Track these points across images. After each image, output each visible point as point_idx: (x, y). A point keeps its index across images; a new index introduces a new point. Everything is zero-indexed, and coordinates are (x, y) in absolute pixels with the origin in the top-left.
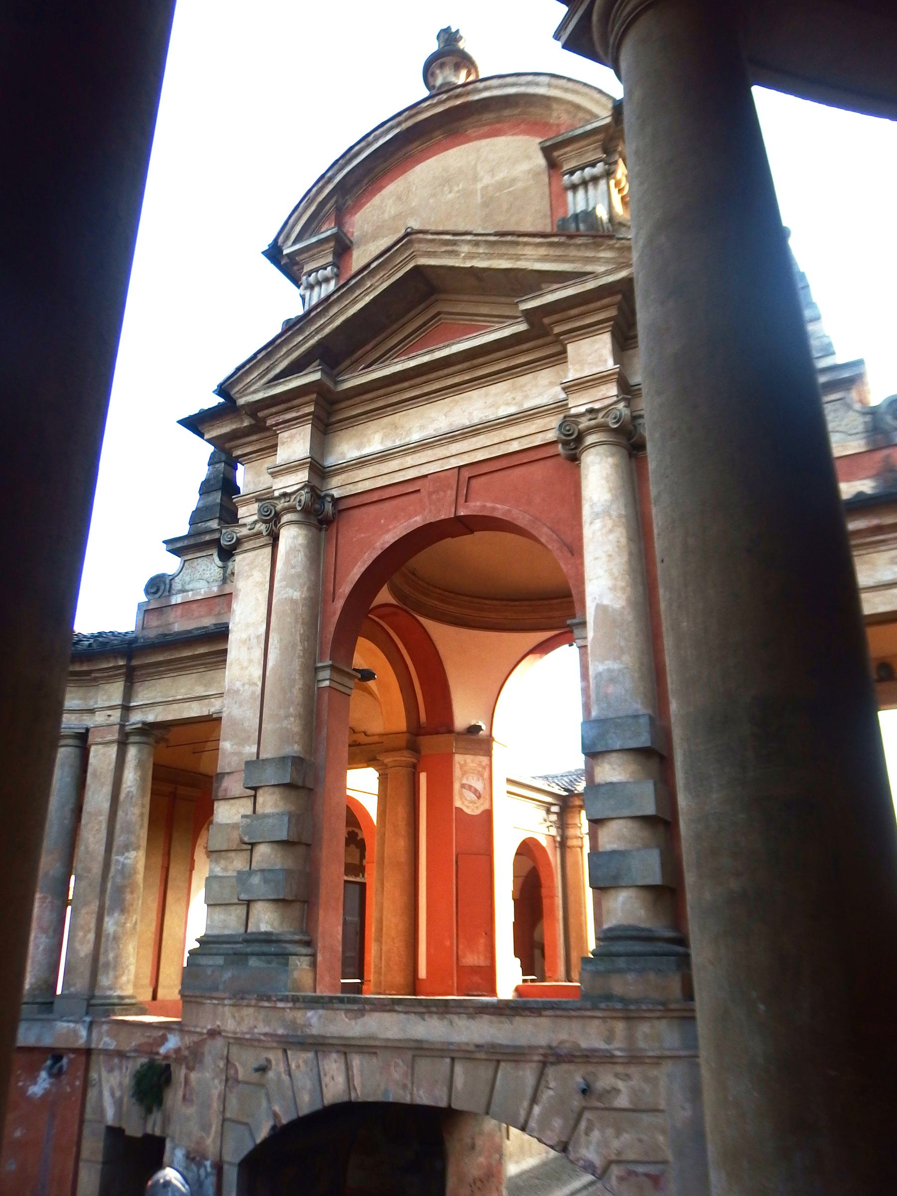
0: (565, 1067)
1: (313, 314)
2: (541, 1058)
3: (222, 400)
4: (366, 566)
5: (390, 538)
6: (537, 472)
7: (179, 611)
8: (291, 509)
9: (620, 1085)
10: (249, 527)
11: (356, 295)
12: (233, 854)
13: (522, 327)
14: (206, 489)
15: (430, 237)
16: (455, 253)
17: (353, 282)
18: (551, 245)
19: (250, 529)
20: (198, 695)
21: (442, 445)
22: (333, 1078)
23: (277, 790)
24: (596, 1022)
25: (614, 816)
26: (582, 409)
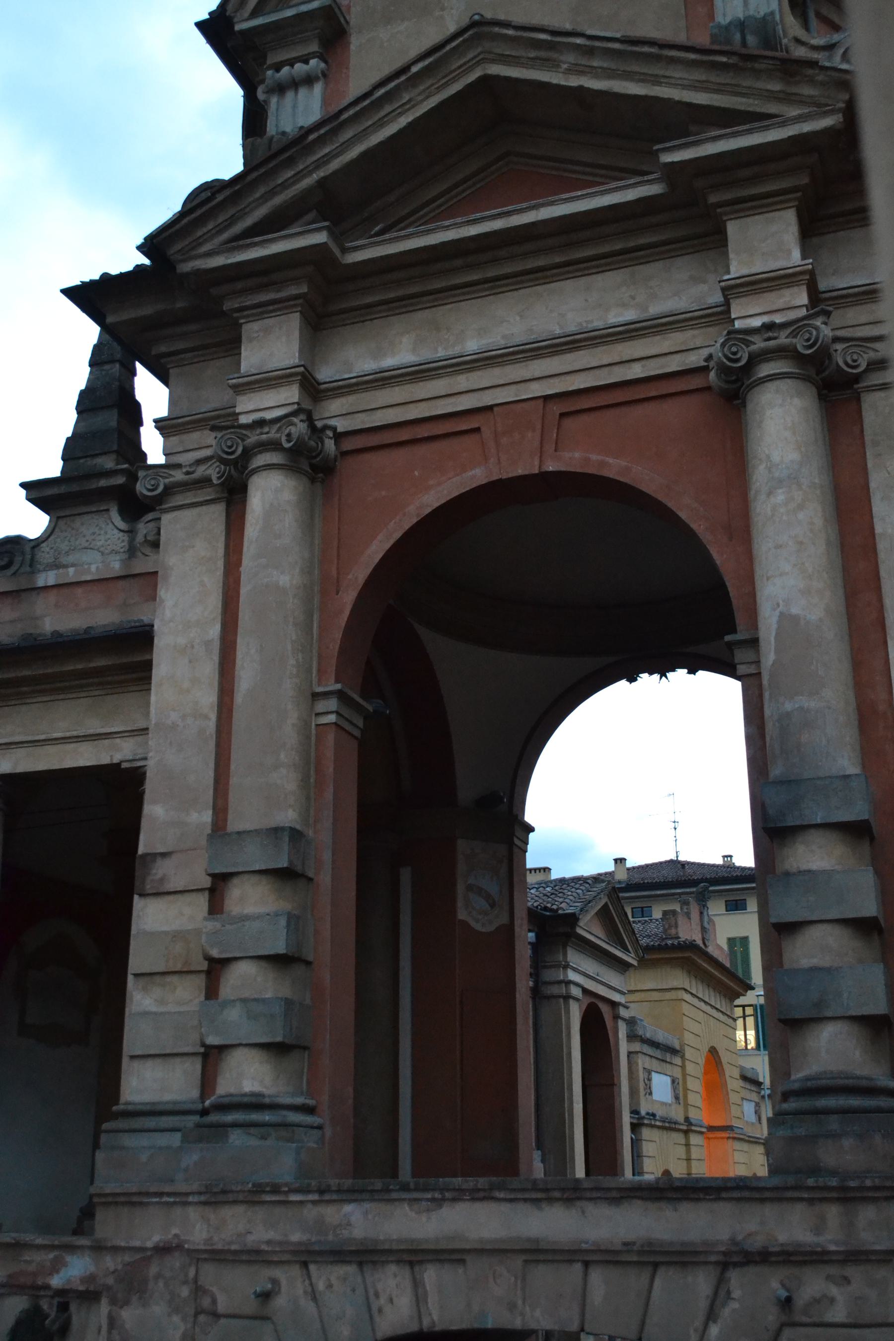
0: (752, 1270)
1: (312, 137)
2: (721, 1258)
3: (146, 261)
4: (392, 542)
5: (432, 499)
6: (673, 414)
7: (52, 597)
8: (273, 446)
9: (834, 1291)
10: (184, 470)
11: (382, 113)
12: (174, 979)
13: (655, 189)
14: (88, 403)
15: (511, 32)
16: (553, 65)
17: (382, 91)
18: (714, 66)
19: (188, 473)
20: (91, 731)
21: (518, 361)
22: (391, 1300)
23: (264, 879)
24: (799, 1207)
25: (814, 918)
26: (757, 322)
